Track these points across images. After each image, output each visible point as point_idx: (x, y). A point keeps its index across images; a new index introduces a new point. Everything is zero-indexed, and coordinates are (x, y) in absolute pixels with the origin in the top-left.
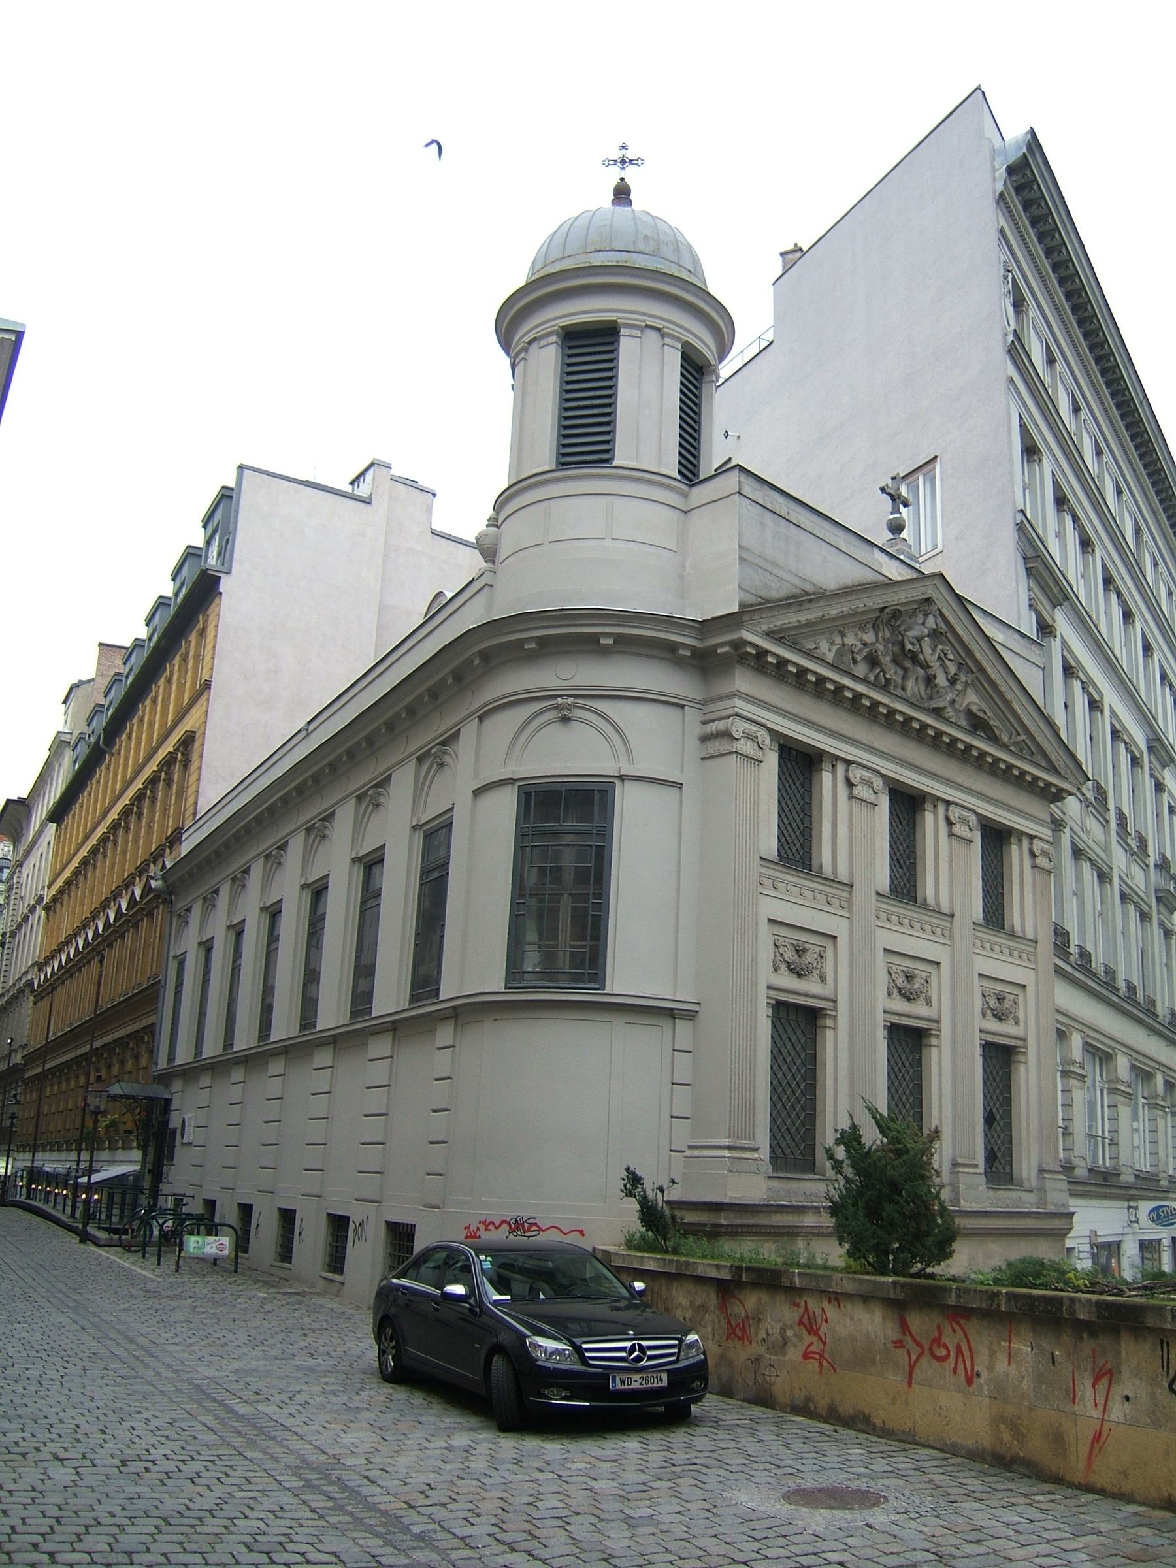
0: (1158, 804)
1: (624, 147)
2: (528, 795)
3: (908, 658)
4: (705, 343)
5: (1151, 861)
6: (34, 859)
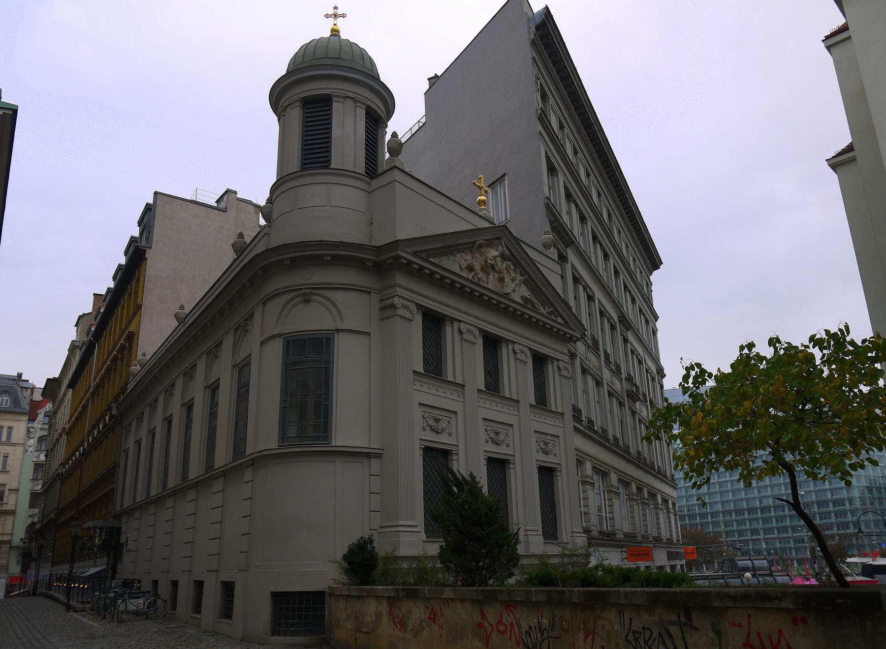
1: (336, 8)
2: (288, 342)
4: (379, 107)
5: (623, 377)
6: (62, 409)
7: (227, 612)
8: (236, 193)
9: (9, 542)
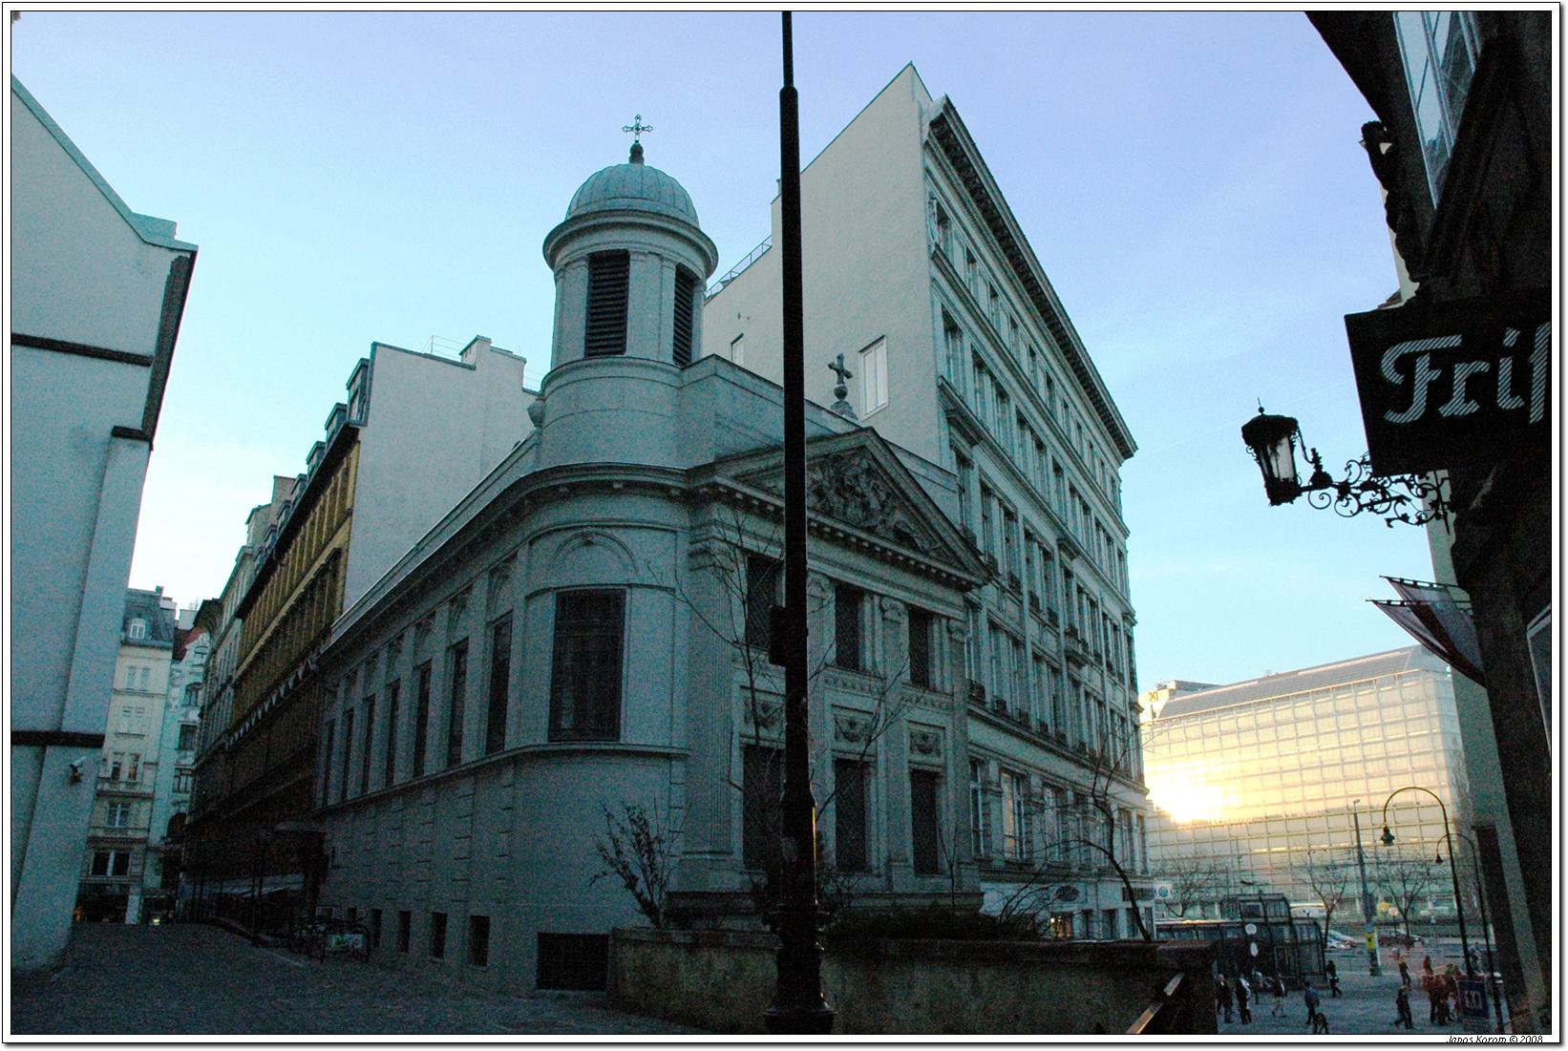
0: (1068, 586)
3: (845, 489)
4: (696, 265)
5: (1062, 631)
6: (226, 644)
7: (479, 954)
8: (488, 341)
9: (145, 841)
